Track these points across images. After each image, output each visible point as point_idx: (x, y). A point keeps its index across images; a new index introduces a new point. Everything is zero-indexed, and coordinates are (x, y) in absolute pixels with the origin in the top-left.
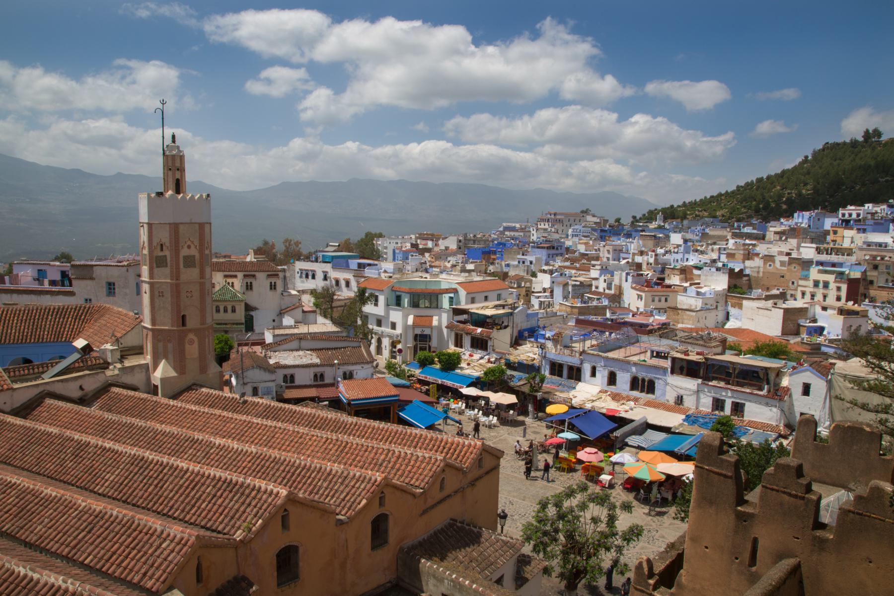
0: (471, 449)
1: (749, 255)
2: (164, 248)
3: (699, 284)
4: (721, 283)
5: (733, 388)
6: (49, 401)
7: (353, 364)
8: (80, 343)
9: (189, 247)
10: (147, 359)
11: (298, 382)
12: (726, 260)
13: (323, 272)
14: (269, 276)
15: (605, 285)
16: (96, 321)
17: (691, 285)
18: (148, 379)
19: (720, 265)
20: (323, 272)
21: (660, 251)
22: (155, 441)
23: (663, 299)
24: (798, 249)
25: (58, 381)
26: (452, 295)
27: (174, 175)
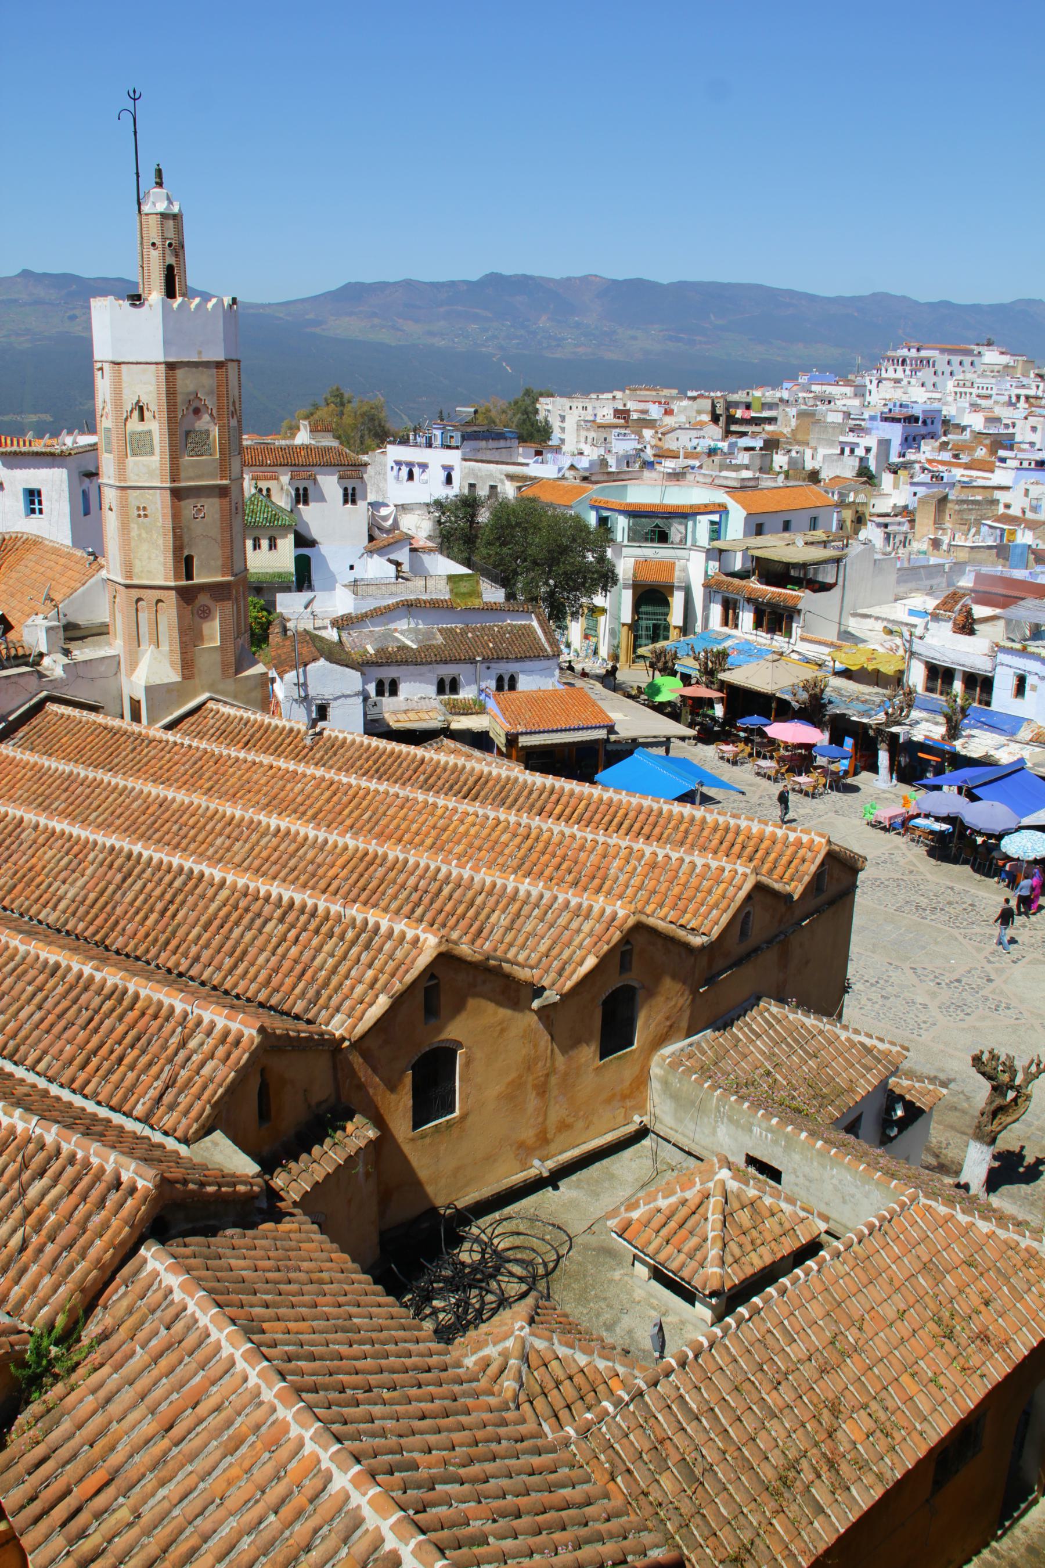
0: (802, 852)
7: (517, 659)
13: (444, 467)
16: (11, 568)
20: (444, 467)
22: (153, 821)
26: (715, 518)
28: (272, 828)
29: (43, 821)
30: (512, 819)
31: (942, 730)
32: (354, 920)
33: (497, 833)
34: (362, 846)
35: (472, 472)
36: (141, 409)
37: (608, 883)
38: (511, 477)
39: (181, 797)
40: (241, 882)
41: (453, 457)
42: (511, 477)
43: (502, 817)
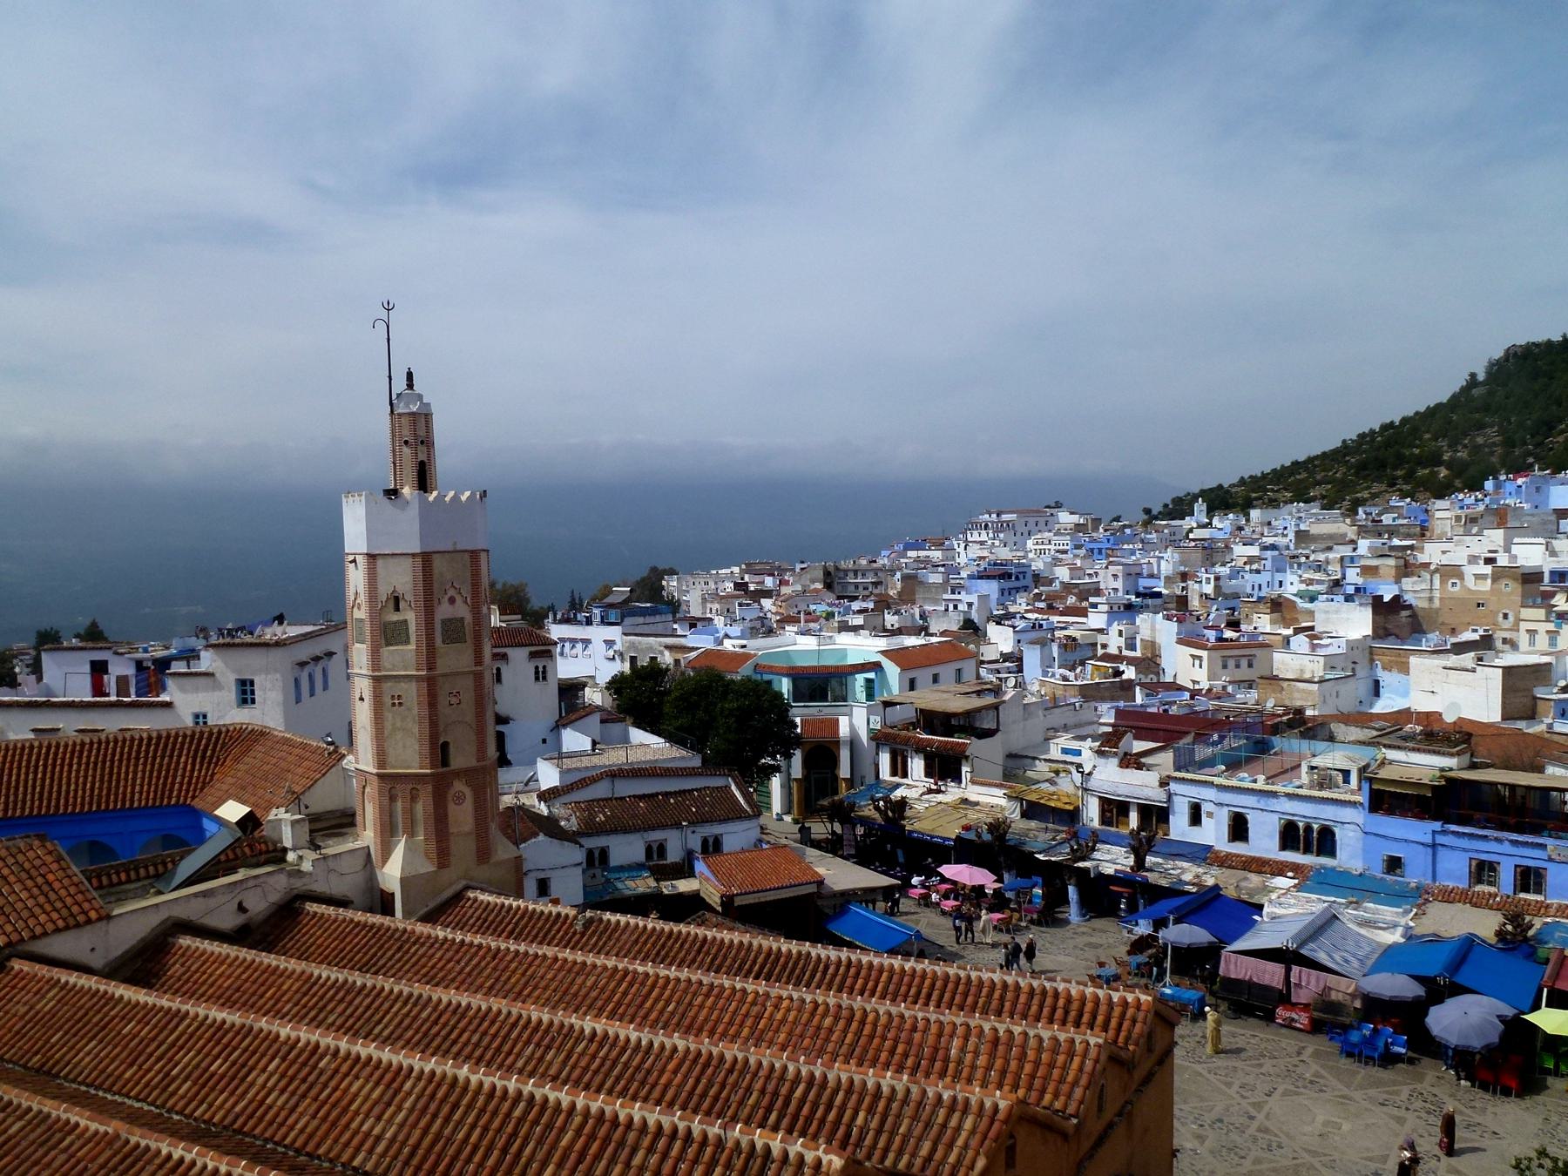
1: (1407, 569)
2: (402, 605)
3: (1312, 628)
4: (1356, 623)
5: (1515, 836)
6: (185, 941)
8: (232, 811)
9: (452, 601)
10: (367, 836)
11: (614, 861)
12: (1360, 581)
14: (533, 655)
15: (1122, 642)
16: (237, 760)
17: (1297, 631)
18: (371, 879)
19: (1350, 590)
21: (1224, 571)
23: (1244, 663)
24: (1507, 550)
25: (196, 895)
26: (871, 675)
28: (587, 1031)
29: (343, 1045)
30: (832, 1001)
31: (1131, 861)
32: (738, 1143)
33: (817, 1018)
34: (693, 1047)
35: (633, 646)
36: (396, 601)
37: (952, 1066)
38: (669, 647)
39: (478, 1001)
40: (595, 1107)
41: (614, 633)
42: (669, 647)
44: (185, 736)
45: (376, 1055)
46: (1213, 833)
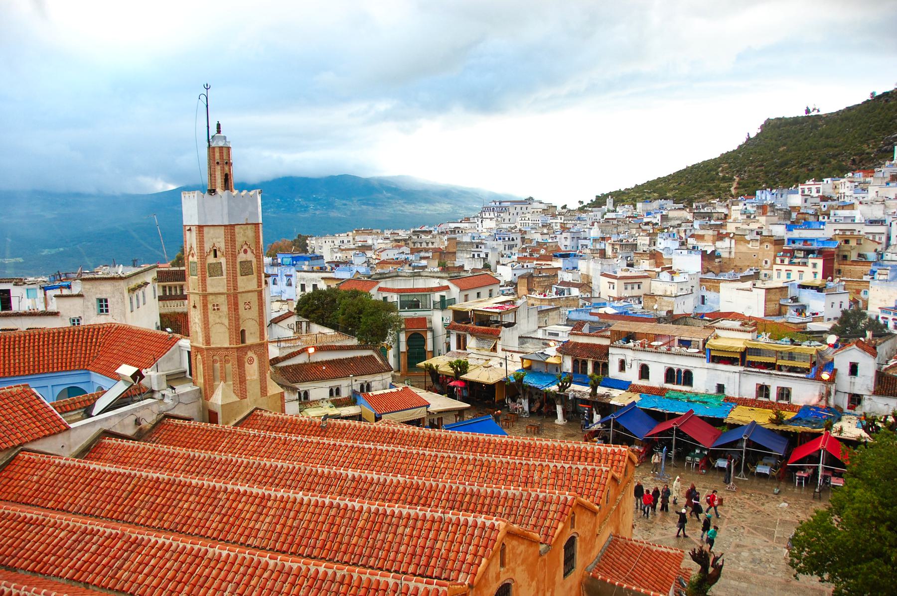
2: (218, 253)
3: (671, 268)
9: (245, 252)
23: (636, 286)
27: (223, 169)
43: (465, 457)
44: (65, 332)
45: (249, 490)
46: (632, 375)
